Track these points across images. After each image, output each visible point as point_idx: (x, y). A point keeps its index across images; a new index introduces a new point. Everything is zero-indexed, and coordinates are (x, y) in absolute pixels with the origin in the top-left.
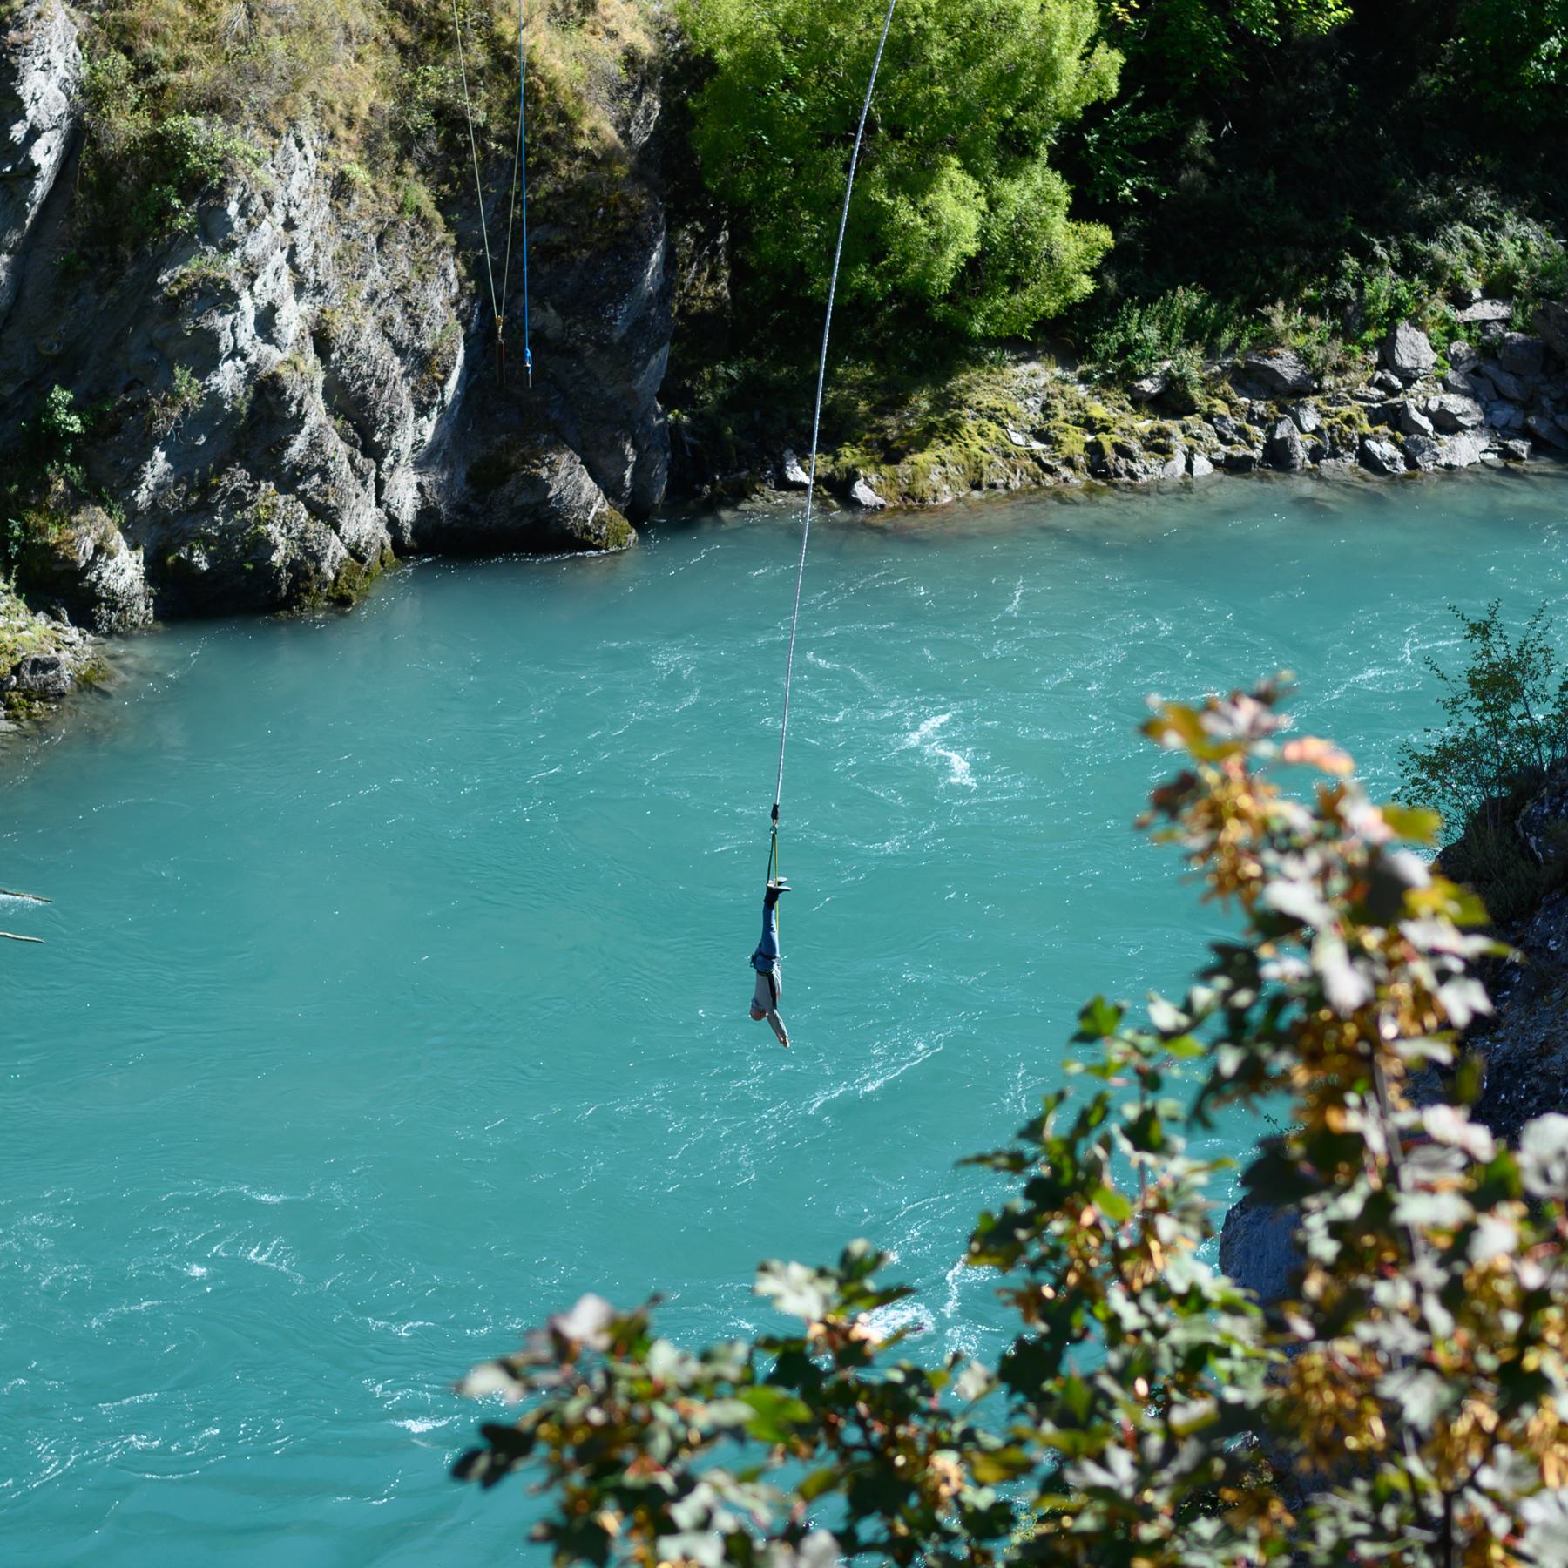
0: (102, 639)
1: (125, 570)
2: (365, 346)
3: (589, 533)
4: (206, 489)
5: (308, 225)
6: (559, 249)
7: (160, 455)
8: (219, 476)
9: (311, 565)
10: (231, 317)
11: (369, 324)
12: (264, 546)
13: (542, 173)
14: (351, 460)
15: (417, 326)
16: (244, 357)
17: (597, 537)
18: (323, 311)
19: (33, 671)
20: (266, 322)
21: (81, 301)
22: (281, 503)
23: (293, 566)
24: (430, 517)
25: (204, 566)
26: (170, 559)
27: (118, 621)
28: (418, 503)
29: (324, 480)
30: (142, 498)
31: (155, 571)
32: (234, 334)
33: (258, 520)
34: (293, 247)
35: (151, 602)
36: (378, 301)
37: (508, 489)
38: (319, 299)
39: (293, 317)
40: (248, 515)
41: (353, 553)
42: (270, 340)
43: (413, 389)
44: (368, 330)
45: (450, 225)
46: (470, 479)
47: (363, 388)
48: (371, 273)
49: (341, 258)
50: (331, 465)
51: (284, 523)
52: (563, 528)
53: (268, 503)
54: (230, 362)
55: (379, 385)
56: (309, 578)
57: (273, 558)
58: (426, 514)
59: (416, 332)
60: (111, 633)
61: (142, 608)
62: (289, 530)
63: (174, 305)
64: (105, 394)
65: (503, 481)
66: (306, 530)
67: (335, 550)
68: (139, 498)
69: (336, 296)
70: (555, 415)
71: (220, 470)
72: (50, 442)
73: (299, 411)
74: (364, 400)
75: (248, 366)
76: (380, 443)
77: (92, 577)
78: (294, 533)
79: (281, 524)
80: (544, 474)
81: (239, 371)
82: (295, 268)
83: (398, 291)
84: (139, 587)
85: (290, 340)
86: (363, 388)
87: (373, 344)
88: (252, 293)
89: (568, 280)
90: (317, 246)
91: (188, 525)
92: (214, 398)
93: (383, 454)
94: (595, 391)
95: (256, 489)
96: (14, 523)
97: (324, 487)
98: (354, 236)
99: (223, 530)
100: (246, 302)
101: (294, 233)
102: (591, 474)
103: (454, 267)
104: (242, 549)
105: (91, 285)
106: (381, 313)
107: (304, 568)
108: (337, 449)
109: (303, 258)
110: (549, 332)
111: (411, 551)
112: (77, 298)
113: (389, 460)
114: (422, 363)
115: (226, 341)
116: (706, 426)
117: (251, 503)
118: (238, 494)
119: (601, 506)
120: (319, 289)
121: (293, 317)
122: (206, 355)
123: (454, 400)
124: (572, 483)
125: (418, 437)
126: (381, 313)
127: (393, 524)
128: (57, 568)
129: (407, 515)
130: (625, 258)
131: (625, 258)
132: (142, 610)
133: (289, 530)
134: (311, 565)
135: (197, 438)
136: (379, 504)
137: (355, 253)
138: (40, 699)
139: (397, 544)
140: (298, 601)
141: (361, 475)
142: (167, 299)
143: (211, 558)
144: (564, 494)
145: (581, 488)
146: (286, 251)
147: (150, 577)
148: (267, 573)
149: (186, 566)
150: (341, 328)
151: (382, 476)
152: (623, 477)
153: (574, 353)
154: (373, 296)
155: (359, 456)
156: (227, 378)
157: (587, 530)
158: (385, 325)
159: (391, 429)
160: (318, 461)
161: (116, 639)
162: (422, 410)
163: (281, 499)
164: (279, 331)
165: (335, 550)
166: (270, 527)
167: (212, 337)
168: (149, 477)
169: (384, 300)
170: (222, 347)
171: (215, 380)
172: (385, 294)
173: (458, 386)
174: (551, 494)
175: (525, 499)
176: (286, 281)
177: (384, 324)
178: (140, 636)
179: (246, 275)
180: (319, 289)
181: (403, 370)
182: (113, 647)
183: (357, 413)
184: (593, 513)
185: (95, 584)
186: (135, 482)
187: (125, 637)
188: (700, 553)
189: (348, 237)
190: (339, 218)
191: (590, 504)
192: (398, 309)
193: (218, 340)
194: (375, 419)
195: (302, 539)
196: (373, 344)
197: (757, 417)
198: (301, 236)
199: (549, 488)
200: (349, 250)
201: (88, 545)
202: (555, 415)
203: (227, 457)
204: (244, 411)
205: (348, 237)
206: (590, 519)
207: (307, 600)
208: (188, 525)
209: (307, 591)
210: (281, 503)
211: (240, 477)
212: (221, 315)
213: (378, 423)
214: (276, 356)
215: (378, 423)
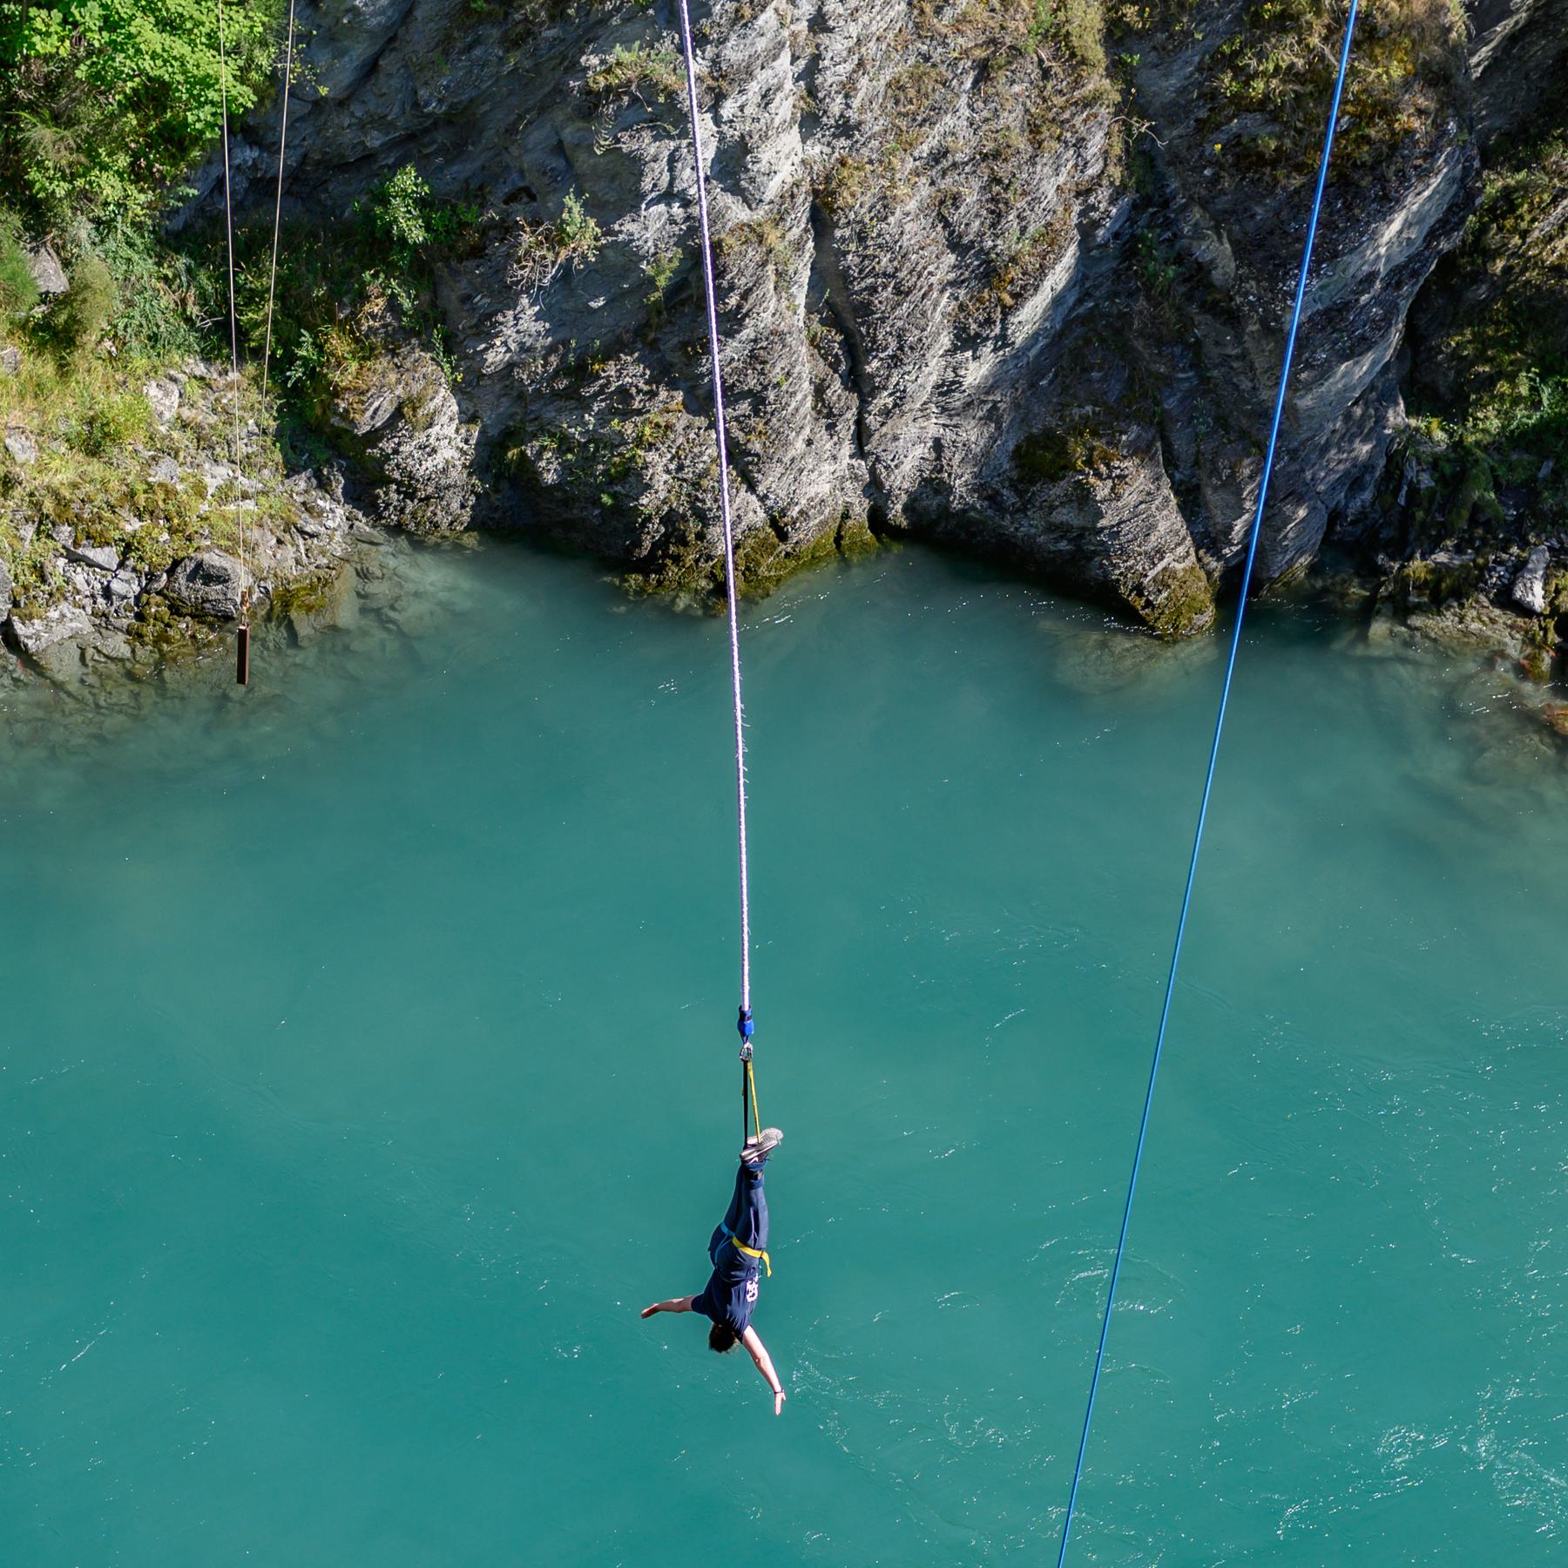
0: (379, 535)
1: (443, 445)
2: (895, 230)
3: (1140, 594)
4: (580, 372)
5: (854, 30)
6: (1260, 160)
7: (528, 309)
8: (604, 361)
9: (693, 526)
10: (672, 145)
11: (914, 198)
12: (631, 477)
13: (1284, 30)
14: (819, 390)
15: (998, 216)
16: (686, 204)
17: (1149, 604)
18: (843, 163)
19: (191, 578)
20: (733, 165)
21: (477, 52)
22: (679, 427)
23: (670, 519)
24: (937, 492)
25: (550, 478)
26: (512, 454)
27: (414, 514)
28: (928, 466)
29: (756, 412)
30: (495, 357)
31: (494, 460)
32: (671, 169)
33: (639, 441)
34: (816, 58)
35: (472, 500)
36: (945, 164)
37: (1057, 490)
38: (843, 142)
39: (785, 159)
40: (629, 429)
41: (774, 523)
42: (736, 190)
43: (962, 307)
44: (912, 206)
45: (1116, 69)
46: (1017, 455)
47: (873, 290)
48: (948, 119)
49: (902, 88)
50: (771, 395)
51: (676, 456)
52: (1106, 574)
53: (661, 421)
54: (662, 207)
55: (898, 291)
56: (685, 544)
57: (644, 501)
58: (933, 485)
59: (993, 225)
60: (397, 530)
61: (455, 505)
62: (680, 468)
63: (591, 103)
64: (476, 194)
65: (1053, 479)
66: (705, 474)
67: (739, 511)
68: (491, 357)
69: (874, 143)
70: (1170, 404)
71: (609, 354)
72: (379, 245)
73: (739, 307)
74: (865, 309)
75: (688, 218)
76: (872, 376)
77: (388, 446)
78: (688, 474)
79: (672, 449)
80: (1102, 490)
81: (672, 221)
82: (812, 91)
83: (985, 157)
84: (457, 475)
85: (772, 189)
86: (873, 290)
87: (909, 224)
88: (717, 120)
89: (1259, 210)
90: (861, 64)
91: (549, 414)
92: (628, 255)
93: (875, 391)
94: (1246, 385)
95: (653, 395)
96: (307, 337)
97: (752, 421)
98: (936, 57)
99: (594, 438)
100: (703, 126)
101: (824, 38)
102: (1182, 508)
103: (1100, 139)
104: (605, 473)
105: (495, 33)
106: (946, 183)
107: (685, 526)
108: (800, 368)
109: (831, 77)
110: (1217, 276)
111: (896, 533)
112: (470, 48)
113: (884, 399)
114: (986, 274)
115: (655, 176)
116: (1456, 468)
117: (639, 412)
118: (624, 393)
119: (1181, 558)
120: (845, 128)
121: (785, 159)
122: (618, 191)
123: (1035, 337)
124: (1141, 514)
125: (950, 375)
126: (946, 183)
127: (874, 487)
128: (335, 421)
129: (903, 476)
130: (1348, 207)
131: (1348, 207)
132: (455, 509)
133: (680, 468)
134: (693, 526)
135: (595, 297)
136: (860, 453)
137: (929, 85)
138: (193, 616)
139: (877, 517)
140: (661, 569)
141: (827, 414)
142: (587, 92)
143: (566, 468)
144: (1125, 528)
145: (1152, 527)
146: (802, 63)
147: (477, 467)
148: (626, 519)
149: (526, 467)
150: (857, 200)
151: (870, 419)
152: (1231, 528)
153: (1233, 319)
154: (938, 156)
155: (837, 385)
156: (650, 228)
157: (1139, 589)
158: (942, 208)
159: (896, 361)
160: (752, 382)
161: (403, 542)
162: (966, 341)
163: (685, 418)
164: (752, 180)
165: (739, 511)
166: (651, 456)
167: (635, 165)
168: (509, 331)
169: (955, 165)
170: (647, 184)
171: (628, 227)
172: (959, 157)
173: (1046, 317)
174: (1103, 523)
175: (1064, 515)
176: (785, 107)
177: (942, 202)
178: (436, 549)
179: (710, 89)
180: (845, 128)
181: (952, 276)
182: (388, 556)
183: (851, 328)
184: (1160, 567)
185: (387, 458)
186: (485, 329)
187: (417, 544)
188: (1301, 677)
189: (927, 58)
190: (917, 26)
191: (1160, 553)
192: (976, 184)
193: (640, 175)
194: (874, 341)
195: (696, 485)
196: (909, 224)
197: (1544, 472)
198: (836, 45)
199: (1100, 515)
200: (917, 79)
201: (385, 405)
202: (1170, 404)
203: (626, 337)
204: (662, 282)
205: (927, 58)
206: (1151, 574)
207: (673, 571)
208: (549, 414)
209: (677, 559)
210: (679, 427)
211: (630, 372)
212: (655, 139)
213: (875, 347)
214: (739, 213)
215: (875, 347)
